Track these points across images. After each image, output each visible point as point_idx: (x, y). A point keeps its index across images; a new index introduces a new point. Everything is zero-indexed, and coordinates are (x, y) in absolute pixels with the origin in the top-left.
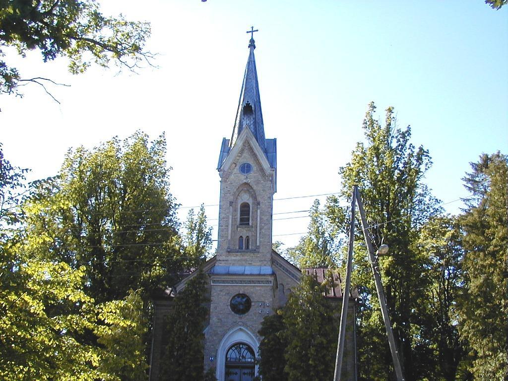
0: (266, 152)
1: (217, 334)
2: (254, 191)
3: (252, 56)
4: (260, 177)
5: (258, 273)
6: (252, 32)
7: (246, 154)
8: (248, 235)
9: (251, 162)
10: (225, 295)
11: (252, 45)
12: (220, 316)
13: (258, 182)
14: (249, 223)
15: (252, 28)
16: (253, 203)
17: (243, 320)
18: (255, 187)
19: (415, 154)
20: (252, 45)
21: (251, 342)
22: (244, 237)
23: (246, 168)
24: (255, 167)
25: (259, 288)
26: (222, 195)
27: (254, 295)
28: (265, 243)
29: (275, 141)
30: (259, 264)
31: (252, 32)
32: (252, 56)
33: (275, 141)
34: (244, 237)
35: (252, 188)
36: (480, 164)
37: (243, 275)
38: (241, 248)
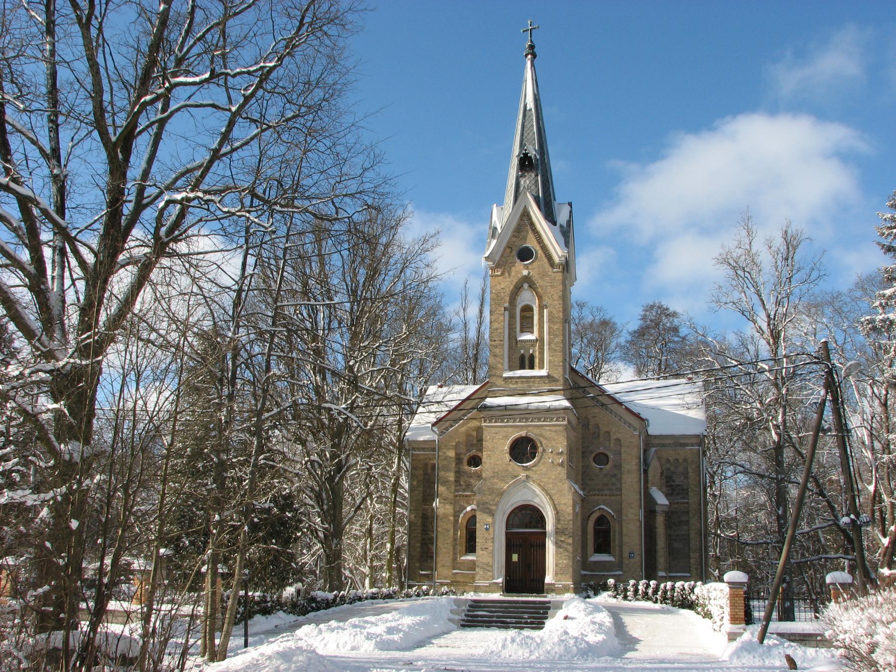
10: (502, 439)
24: (540, 252)
28: (555, 364)
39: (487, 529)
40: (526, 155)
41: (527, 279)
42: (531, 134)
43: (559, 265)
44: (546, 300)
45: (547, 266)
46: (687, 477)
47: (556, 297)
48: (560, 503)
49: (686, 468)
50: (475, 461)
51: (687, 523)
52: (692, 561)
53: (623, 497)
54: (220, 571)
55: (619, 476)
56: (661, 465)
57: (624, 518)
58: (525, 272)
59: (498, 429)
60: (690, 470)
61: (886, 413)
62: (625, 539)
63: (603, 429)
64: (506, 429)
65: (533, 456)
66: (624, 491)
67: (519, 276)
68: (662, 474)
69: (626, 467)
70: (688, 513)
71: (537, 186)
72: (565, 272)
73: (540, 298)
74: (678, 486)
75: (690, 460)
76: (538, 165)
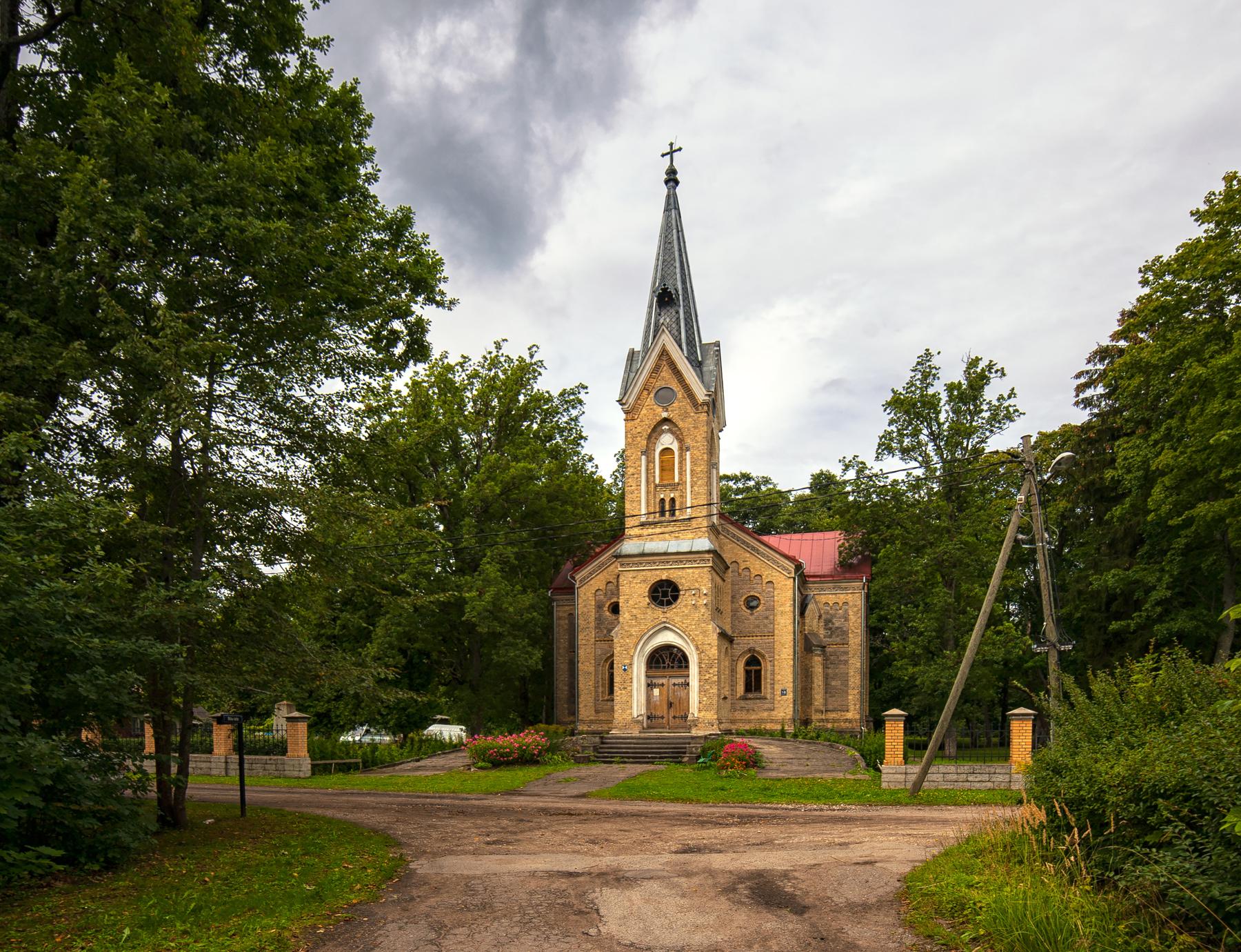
0: (698, 365)
1: (631, 635)
2: (680, 429)
3: (672, 204)
4: (688, 407)
5: (688, 550)
6: (671, 153)
7: (666, 373)
8: (672, 496)
9: (675, 385)
11: (672, 178)
12: (635, 611)
13: (685, 416)
14: (142, 744)
15: (671, 145)
16: (681, 449)
17: (668, 615)
18: (681, 424)
19: (507, 477)
20: (672, 178)
21: (684, 644)
22: (667, 500)
23: (664, 396)
24: (680, 394)
25: (691, 571)
26: (630, 440)
27: (683, 581)
29: (717, 344)
30: (691, 536)
31: (671, 153)
32: (672, 204)
33: (717, 344)
34: (667, 500)
35: (677, 426)
36: (1229, 545)
37: (665, 554)
38: (662, 513)
39: (625, 670)
40: (665, 290)
41: (666, 420)
42: (672, 268)
43: (705, 404)
44: (689, 442)
45: (689, 408)
46: (847, 619)
47: (699, 438)
48: (703, 644)
49: (846, 611)
50: (615, 609)
51: (846, 662)
52: (850, 697)
53: (776, 638)
54: (180, 700)
55: (771, 617)
56: (819, 610)
57: (777, 657)
58: (665, 415)
59: (634, 574)
60: (851, 613)
61: (497, 793)
62: (778, 677)
63: (754, 573)
64: (644, 573)
65: (665, 654)
66: (776, 632)
67: (658, 419)
68: (820, 617)
69: (779, 609)
70: (846, 653)
71: (678, 324)
72: (711, 414)
73: (681, 441)
74: (837, 628)
75: (851, 604)
76: (678, 299)
